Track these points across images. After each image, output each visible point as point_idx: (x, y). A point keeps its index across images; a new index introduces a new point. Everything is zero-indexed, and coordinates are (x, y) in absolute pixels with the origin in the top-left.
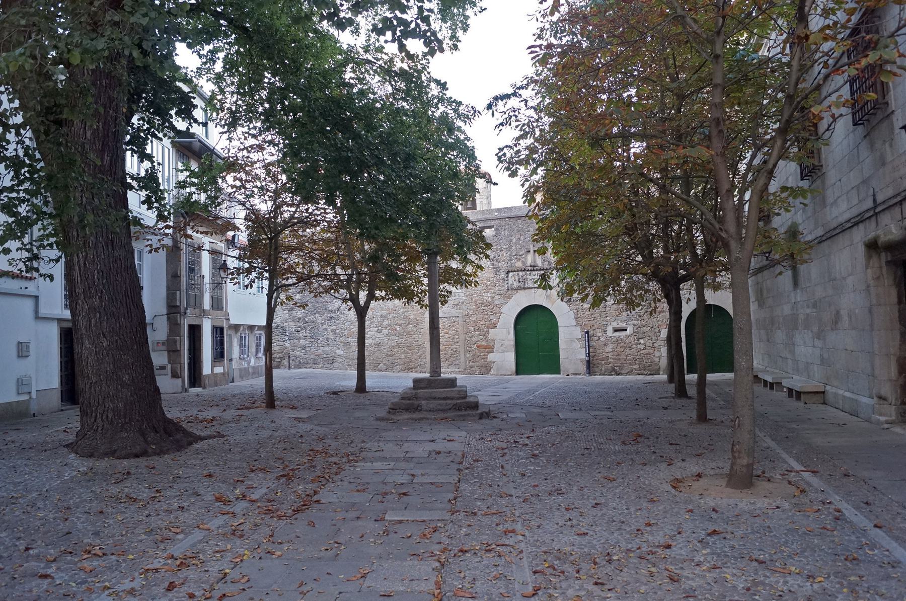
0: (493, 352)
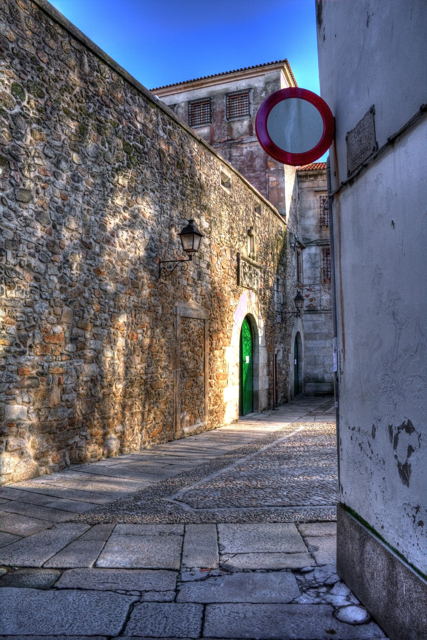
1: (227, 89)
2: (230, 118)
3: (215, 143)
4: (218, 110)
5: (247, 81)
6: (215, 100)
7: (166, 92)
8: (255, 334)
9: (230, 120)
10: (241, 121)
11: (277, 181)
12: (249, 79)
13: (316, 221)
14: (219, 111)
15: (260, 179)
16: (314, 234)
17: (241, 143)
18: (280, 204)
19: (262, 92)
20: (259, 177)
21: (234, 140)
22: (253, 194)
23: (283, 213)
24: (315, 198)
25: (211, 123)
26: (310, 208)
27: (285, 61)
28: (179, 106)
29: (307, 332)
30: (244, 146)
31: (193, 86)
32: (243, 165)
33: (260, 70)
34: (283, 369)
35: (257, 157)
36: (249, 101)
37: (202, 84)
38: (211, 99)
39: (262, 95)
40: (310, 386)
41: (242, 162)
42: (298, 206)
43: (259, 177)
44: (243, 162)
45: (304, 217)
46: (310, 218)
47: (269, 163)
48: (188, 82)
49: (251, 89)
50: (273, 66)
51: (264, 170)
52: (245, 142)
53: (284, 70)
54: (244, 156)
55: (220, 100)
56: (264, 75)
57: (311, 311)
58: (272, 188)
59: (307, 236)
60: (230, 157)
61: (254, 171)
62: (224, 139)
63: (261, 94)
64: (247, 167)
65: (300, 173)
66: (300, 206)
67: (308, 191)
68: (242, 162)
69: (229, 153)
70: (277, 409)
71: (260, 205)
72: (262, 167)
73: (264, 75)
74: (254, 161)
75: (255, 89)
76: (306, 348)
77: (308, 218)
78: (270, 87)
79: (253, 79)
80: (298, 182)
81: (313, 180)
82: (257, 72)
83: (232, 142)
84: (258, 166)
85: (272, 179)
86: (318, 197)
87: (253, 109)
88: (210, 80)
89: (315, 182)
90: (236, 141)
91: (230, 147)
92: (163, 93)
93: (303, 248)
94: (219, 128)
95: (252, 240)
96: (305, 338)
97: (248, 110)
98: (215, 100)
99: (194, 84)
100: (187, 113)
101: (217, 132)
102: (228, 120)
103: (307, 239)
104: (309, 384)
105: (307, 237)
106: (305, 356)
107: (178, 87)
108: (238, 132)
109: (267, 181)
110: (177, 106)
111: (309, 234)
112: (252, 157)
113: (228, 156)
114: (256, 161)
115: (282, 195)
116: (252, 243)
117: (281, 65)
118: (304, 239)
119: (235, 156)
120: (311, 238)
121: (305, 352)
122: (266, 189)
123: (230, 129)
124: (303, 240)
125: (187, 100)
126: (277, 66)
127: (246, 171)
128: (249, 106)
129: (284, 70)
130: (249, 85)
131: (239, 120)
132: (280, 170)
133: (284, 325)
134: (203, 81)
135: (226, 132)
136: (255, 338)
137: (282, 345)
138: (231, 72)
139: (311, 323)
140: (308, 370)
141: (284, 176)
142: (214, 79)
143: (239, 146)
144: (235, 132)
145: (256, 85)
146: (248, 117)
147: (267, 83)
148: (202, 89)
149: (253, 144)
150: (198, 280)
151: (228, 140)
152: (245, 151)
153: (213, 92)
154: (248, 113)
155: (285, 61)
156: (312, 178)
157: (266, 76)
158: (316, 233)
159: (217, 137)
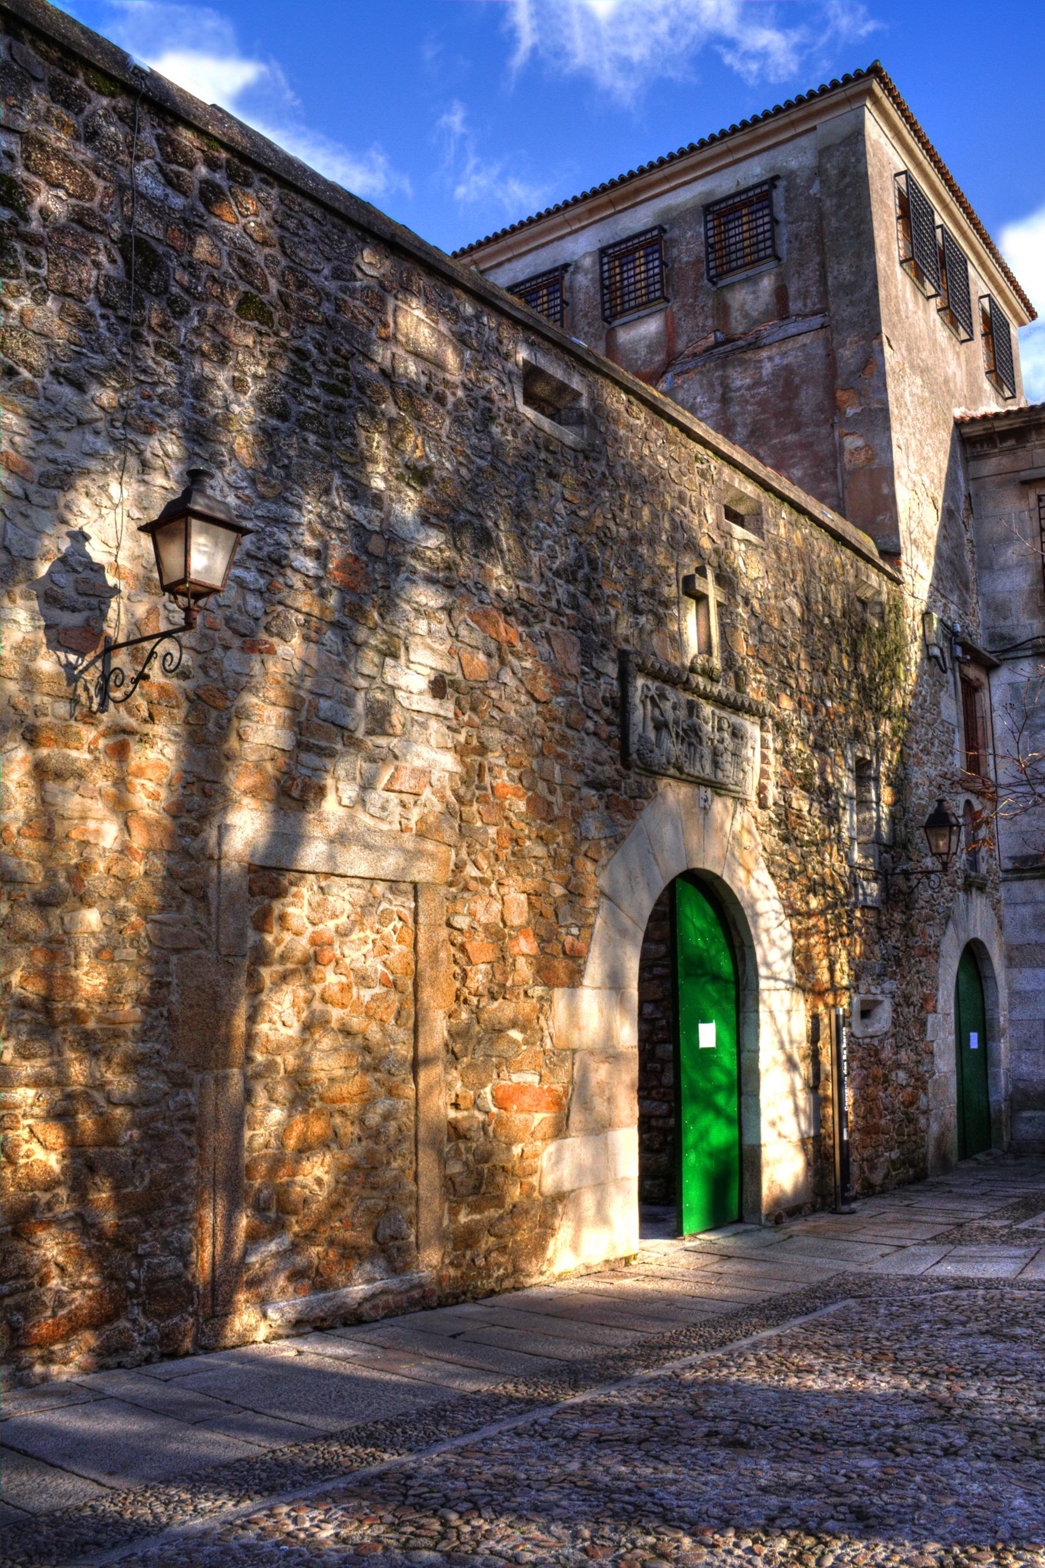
1: (710, 193)
2: (720, 276)
3: (680, 360)
4: (685, 259)
5: (765, 158)
6: (676, 232)
7: (542, 234)
8: (742, 944)
9: (721, 284)
10: (752, 280)
11: (867, 446)
12: (771, 153)
13: (1029, 578)
14: (688, 263)
15: (816, 448)
16: (1025, 619)
17: (756, 345)
18: (880, 518)
19: (810, 181)
20: (811, 444)
21: (734, 340)
22: (715, 463)
23: (889, 547)
24: (1023, 505)
25: (667, 300)
26: (1008, 539)
27: (875, 71)
28: (578, 268)
29: (1016, 942)
30: (764, 354)
31: (612, 203)
32: (763, 412)
33: (800, 114)
34: (898, 1066)
35: (803, 381)
36: (771, 214)
37: (638, 191)
38: (665, 231)
39: (812, 192)
40: (1030, 1119)
41: (758, 403)
42: (968, 536)
43: (811, 444)
44: (763, 403)
45: (990, 568)
46: (1009, 568)
47: (839, 394)
48: (595, 193)
49: (777, 177)
50: (839, 95)
51: (826, 420)
52: (764, 341)
53: (877, 102)
54: (766, 383)
55: (690, 229)
56: (814, 128)
57: (1022, 871)
58: (854, 473)
59: (1004, 626)
60: (724, 394)
61: (797, 428)
62: (704, 344)
63: (810, 187)
64: (776, 416)
65: (966, 430)
66: (977, 532)
67: (1001, 485)
68: (758, 403)
69: (722, 384)
70: (845, 1208)
71: (759, 505)
72: (822, 411)
73: (814, 128)
74: (796, 396)
75: (791, 175)
76: (1013, 994)
77: (1002, 569)
78: (834, 161)
79: (782, 148)
80: (967, 460)
81: (1011, 450)
82: (793, 124)
83: (728, 347)
84: (807, 410)
85: (852, 442)
86: (1033, 499)
87: (785, 238)
88: (658, 175)
89: (1020, 453)
90: (740, 343)
91: (724, 362)
92: (533, 238)
93: (990, 668)
94: (690, 311)
95: (702, 611)
96: (1011, 962)
97: (768, 243)
98: (676, 232)
99: (614, 194)
100: (598, 286)
101: (686, 325)
102: (714, 284)
103: (1002, 637)
104: (1026, 1114)
105: (1005, 631)
106: (1011, 1021)
107: (569, 214)
108: (746, 316)
109: (837, 452)
110: (571, 269)
111: (1009, 622)
112: (788, 383)
113: (719, 391)
114: (803, 394)
115: (886, 491)
116: (703, 623)
117: (861, 87)
118: (995, 637)
119: (740, 388)
120: (1016, 633)
121: (1012, 1007)
122: (835, 478)
123: (723, 311)
124: (992, 639)
125: (599, 246)
126: (849, 92)
127: (773, 430)
128: (772, 230)
129: (877, 102)
130: (772, 169)
131: (747, 280)
132: (876, 410)
133: (898, 917)
134: (637, 183)
135: (710, 322)
136: (743, 958)
137: (889, 985)
138: (713, 139)
139: (1026, 911)
140: (1025, 1068)
141: (888, 429)
142: (667, 171)
143: (749, 355)
144: (735, 315)
145: (793, 164)
146: (773, 264)
147: (824, 152)
148: (639, 208)
149: (790, 345)
150: (370, 732)
151: (717, 344)
152: (767, 368)
153: (669, 210)
154: (769, 251)
155: (875, 71)
156: (1011, 443)
157: (819, 131)
158: (1033, 615)
159: (685, 338)
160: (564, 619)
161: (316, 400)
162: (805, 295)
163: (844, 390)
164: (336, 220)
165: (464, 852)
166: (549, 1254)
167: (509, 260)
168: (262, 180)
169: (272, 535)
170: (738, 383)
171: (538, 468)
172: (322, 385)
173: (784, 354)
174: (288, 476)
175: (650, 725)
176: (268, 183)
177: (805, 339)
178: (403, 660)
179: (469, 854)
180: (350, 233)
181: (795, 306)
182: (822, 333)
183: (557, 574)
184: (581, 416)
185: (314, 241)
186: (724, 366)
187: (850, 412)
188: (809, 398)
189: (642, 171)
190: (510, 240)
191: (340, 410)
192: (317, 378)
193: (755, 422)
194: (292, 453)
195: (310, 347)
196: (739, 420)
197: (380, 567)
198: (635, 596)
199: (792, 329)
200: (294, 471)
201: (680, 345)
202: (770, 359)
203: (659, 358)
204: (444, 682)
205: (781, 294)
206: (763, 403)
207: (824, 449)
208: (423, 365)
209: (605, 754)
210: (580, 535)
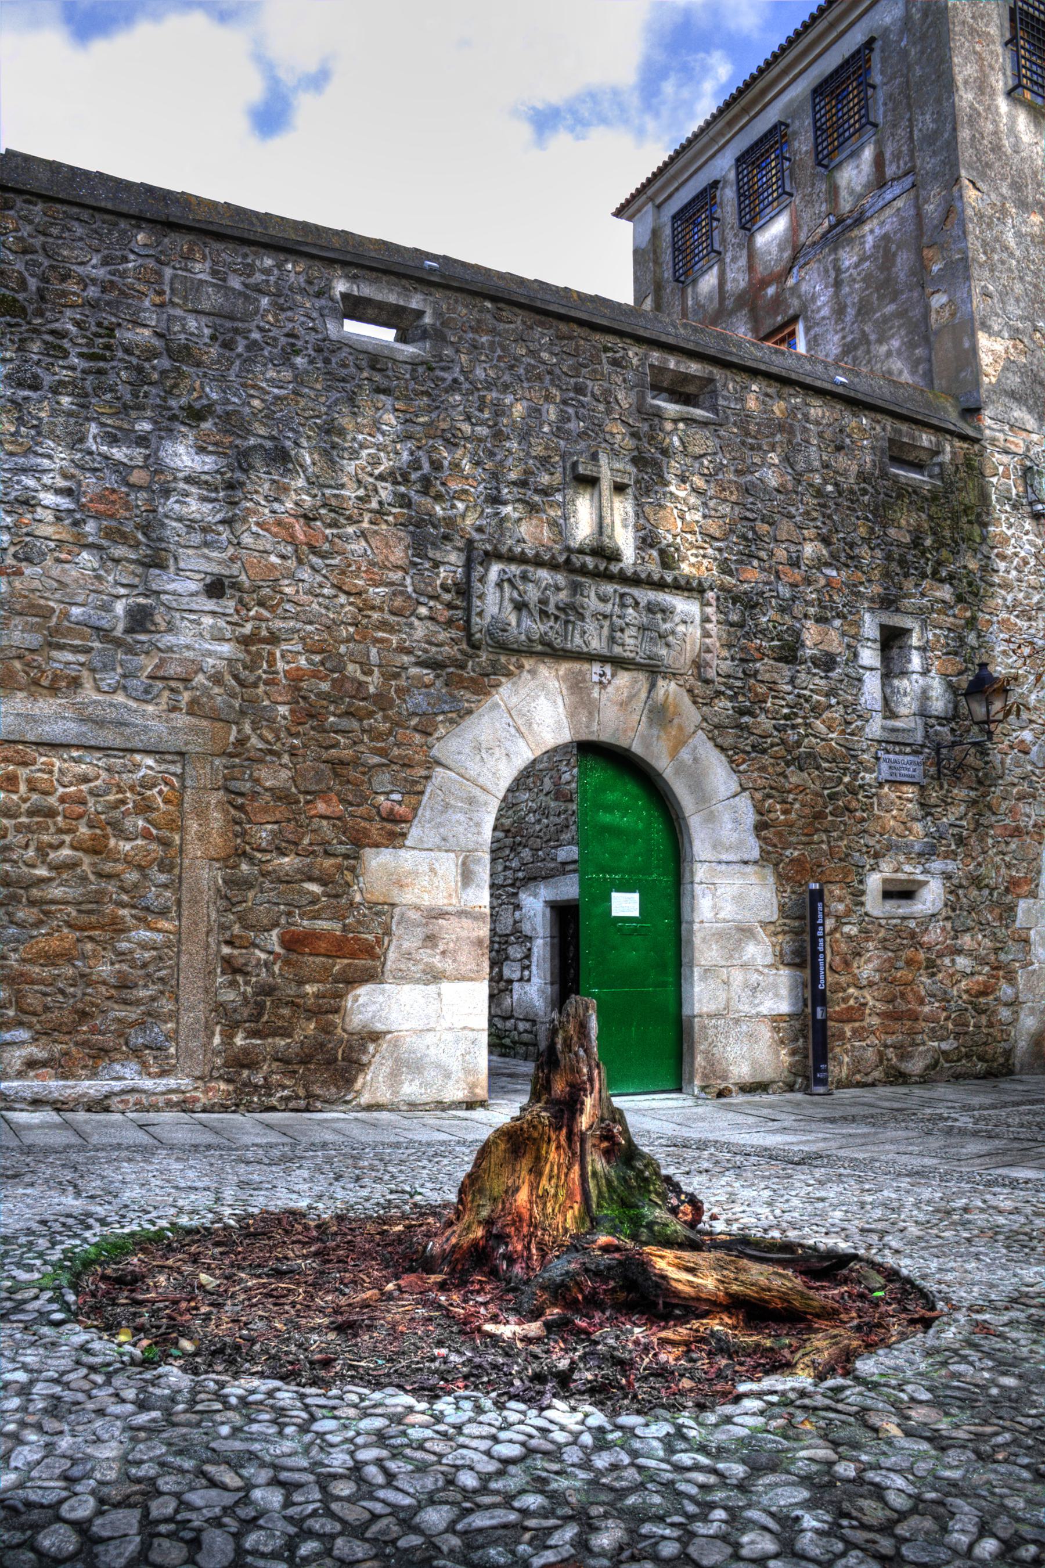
0: (372, 976)
17: (860, 221)
30: (867, 228)
31: (745, 110)
35: (899, 248)
37: (764, 92)
41: (864, 280)
43: (906, 311)
62: (820, 230)
74: (894, 265)
83: (839, 229)
88: (776, 71)
94: (809, 202)
99: (744, 102)
101: (806, 216)
108: (852, 192)
112: (887, 250)
113: (833, 274)
115: (967, 345)
123: (833, 191)
134: (761, 85)
143: (856, 232)
144: (844, 193)
149: (888, 212)
151: (832, 228)
152: (870, 240)
159: (805, 229)
160: (391, 518)
161: (73, 368)
162: (897, 157)
163: (929, 247)
164: (107, 217)
165: (247, 728)
166: (358, 1085)
167: (677, 189)
168: (25, 201)
169: (18, 482)
170: (847, 263)
171: (360, 386)
172: (81, 355)
173: (882, 223)
174: (39, 434)
175: (508, 606)
176: (30, 202)
177: (899, 203)
178: (172, 569)
179: (254, 730)
180: (123, 224)
181: (890, 171)
182: (912, 193)
183: (381, 478)
184: (425, 331)
185: (81, 239)
186: (835, 250)
187: (935, 268)
188: (903, 261)
189: (761, 71)
190: (672, 171)
191: (100, 372)
192: (74, 351)
193: (861, 300)
194: (42, 415)
195: (70, 326)
196: (849, 301)
197: (143, 495)
198: (497, 489)
199: (889, 196)
200: (45, 429)
201: (802, 237)
202: (872, 231)
203: (787, 254)
204: (222, 584)
205: (879, 162)
206: (867, 279)
207: (916, 313)
208: (204, 320)
209: (443, 636)
210: (419, 440)
